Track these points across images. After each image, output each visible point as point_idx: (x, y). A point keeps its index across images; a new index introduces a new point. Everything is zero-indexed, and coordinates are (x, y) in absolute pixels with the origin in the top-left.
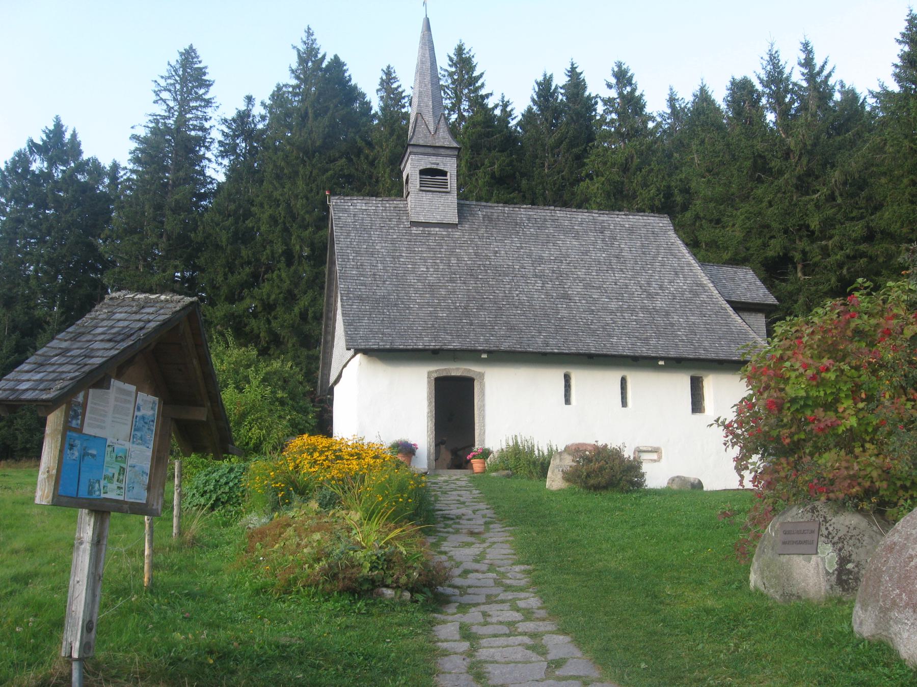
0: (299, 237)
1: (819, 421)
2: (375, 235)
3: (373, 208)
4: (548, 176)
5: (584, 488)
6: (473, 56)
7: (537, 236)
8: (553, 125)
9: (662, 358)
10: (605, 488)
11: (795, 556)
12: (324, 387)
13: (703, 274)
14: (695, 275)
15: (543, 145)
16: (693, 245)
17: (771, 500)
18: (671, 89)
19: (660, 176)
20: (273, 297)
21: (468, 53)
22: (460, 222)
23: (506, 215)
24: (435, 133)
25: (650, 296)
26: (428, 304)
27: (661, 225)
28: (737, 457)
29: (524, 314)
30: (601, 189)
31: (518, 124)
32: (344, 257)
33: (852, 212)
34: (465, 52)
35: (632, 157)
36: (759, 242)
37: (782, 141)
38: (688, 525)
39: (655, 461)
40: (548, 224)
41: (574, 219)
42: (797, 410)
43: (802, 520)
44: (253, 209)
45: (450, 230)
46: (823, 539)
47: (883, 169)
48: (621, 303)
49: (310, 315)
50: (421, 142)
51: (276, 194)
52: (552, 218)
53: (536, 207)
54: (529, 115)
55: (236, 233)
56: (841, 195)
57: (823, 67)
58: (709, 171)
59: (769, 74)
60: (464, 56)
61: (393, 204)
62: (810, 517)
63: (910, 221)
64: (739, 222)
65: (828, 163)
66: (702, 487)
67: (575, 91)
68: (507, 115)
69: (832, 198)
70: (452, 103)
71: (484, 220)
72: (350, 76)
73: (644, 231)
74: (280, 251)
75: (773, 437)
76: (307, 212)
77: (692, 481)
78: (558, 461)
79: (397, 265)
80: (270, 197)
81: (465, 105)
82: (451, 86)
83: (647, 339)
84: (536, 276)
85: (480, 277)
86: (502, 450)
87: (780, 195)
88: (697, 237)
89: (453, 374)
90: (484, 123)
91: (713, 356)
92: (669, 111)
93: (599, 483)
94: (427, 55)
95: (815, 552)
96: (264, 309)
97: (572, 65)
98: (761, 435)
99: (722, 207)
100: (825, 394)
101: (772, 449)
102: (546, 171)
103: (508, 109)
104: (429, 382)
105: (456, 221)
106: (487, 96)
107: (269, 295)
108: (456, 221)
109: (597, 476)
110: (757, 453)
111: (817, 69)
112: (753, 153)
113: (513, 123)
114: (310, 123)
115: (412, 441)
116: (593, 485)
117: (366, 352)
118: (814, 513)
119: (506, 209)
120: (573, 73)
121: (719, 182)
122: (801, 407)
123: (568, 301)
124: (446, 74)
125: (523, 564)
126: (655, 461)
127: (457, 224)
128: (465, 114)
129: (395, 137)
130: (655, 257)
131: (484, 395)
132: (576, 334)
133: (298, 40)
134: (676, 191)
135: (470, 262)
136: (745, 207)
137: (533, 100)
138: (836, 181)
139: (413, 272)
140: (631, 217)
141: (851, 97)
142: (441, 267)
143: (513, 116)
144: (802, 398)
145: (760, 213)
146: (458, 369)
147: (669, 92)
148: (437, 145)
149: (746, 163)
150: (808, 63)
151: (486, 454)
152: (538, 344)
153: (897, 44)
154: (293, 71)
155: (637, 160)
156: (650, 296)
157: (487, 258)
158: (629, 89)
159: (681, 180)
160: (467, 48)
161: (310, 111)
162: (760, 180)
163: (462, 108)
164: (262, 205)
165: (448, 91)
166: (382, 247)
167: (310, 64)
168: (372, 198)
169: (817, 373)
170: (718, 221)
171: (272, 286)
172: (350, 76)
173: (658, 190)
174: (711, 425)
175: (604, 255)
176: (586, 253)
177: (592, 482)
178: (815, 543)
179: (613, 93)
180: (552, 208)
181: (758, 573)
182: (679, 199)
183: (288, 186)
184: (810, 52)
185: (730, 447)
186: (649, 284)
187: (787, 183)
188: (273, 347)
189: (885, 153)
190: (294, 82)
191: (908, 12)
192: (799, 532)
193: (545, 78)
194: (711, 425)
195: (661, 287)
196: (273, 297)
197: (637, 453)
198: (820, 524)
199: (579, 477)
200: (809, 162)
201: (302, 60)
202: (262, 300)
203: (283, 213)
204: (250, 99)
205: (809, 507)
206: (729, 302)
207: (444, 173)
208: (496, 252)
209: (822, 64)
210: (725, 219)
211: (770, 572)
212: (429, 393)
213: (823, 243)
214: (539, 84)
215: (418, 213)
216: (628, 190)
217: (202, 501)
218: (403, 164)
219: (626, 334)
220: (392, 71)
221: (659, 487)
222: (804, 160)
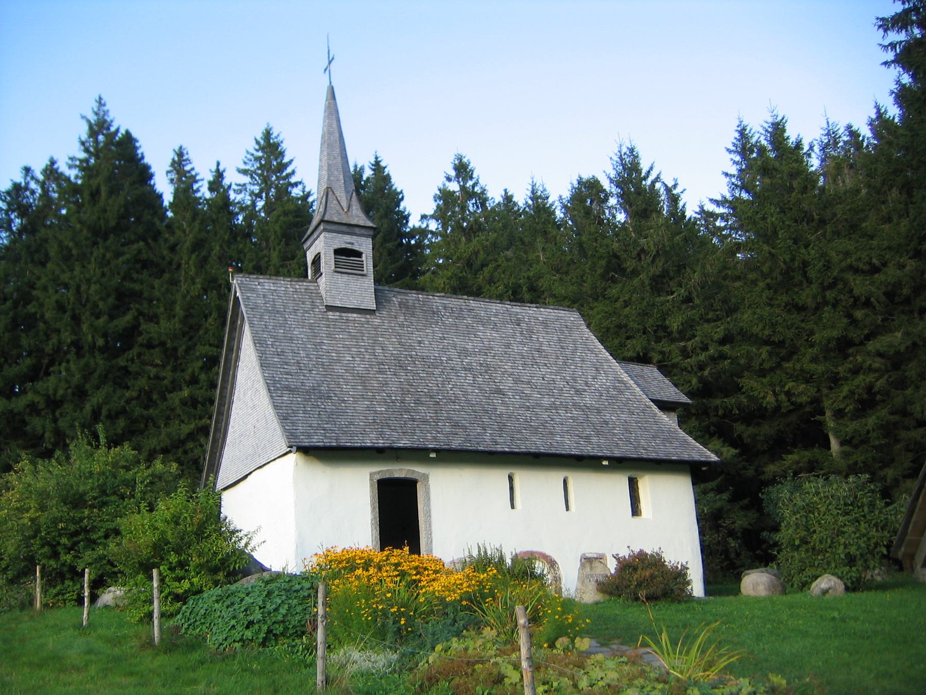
0: (91, 325)
3: (283, 289)
6: (282, 142)
9: (606, 458)
13: (622, 371)
20: (61, 392)
24: (348, 210)
25: (578, 392)
27: (572, 319)
32: (262, 342)
33: (708, 314)
40: (465, 313)
44: (34, 293)
48: (553, 400)
49: (104, 412)
50: (336, 219)
51: (65, 277)
55: (14, 319)
57: (649, 172)
61: (301, 286)
63: (772, 323)
69: (688, 300)
73: (557, 325)
76: (102, 299)
79: (320, 353)
89: (396, 476)
91: (653, 455)
96: (48, 406)
97: (377, 158)
104: (371, 485)
105: (374, 307)
108: (374, 307)
111: (643, 174)
117: (307, 451)
119: (420, 296)
123: (502, 396)
127: (374, 311)
129: (198, 222)
139: (339, 361)
140: (542, 309)
142: (367, 357)
146: (401, 470)
148: (352, 223)
149: (600, 262)
154: (83, 143)
155: (482, 255)
156: (578, 392)
162: (614, 281)
164: (45, 288)
166: (301, 333)
168: (279, 278)
171: (60, 380)
173: (506, 286)
176: (508, 346)
180: (465, 297)
183: (78, 269)
186: (575, 380)
191: (737, 123)
195: (586, 384)
196: (61, 392)
201: (93, 133)
202: (48, 396)
203: (72, 300)
204: (27, 170)
206: (652, 400)
207: (358, 254)
208: (420, 342)
209: (648, 169)
212: (372, 497)
213: (682, 344)
217: (248, 634)
219: (567, 432)
220: (185, 152)
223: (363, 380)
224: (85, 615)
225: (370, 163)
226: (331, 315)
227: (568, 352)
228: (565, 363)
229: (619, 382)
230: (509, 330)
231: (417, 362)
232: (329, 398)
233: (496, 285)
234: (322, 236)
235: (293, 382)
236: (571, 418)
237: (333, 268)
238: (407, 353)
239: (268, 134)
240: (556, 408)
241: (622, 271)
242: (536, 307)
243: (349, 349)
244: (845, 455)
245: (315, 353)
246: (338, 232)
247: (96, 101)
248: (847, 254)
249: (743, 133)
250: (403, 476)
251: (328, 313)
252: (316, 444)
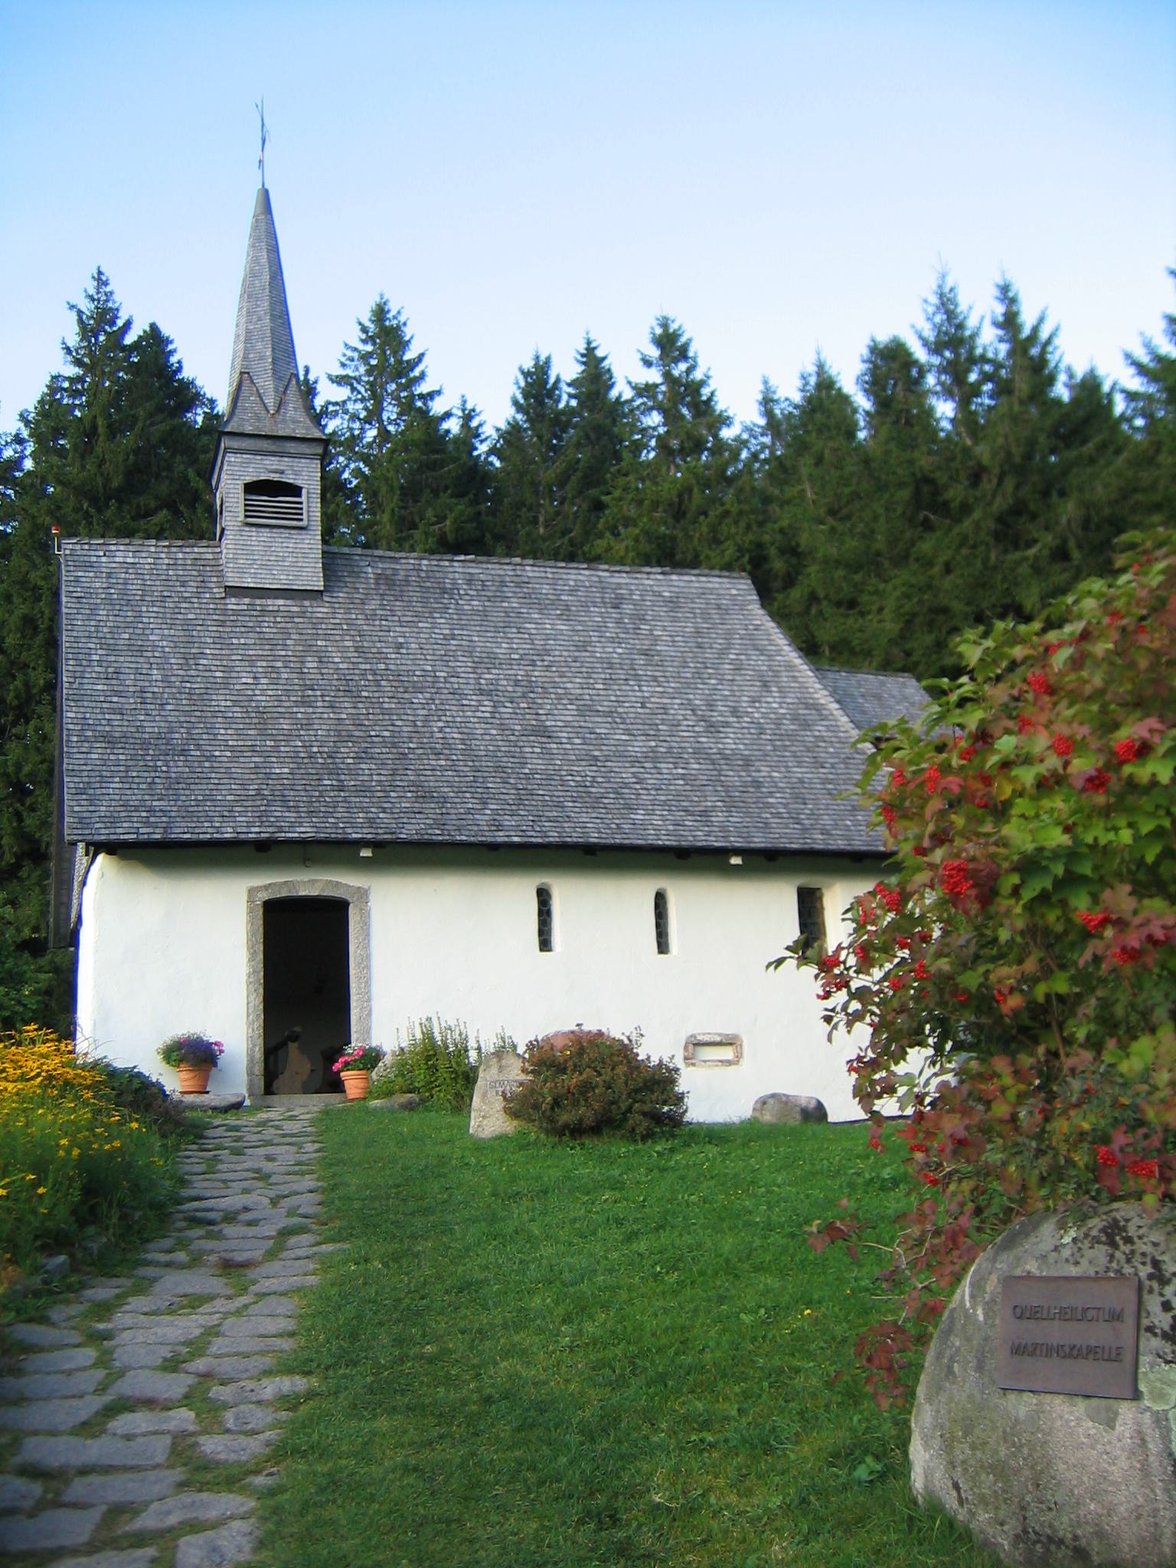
1: (1121, 924)
2: (150, 614)
3: (150, 560)
4: (544, 540)
5: (547, 1132)
6: (405, 324)
7: (485, 614)
8: (553, 448)
9: (737, 852)
10: (596, 1130)
11: (1058, 1400)
12: (62, 931)
13: (818, 686)
14: (803, 687)
15: (534, 484)
16: (810, 649)
17: (967, 1186)
18: (766, 382)
19: (742, 524)
21: (395, 317)
22: (328, 588)
23: (423, 574)
24: (278, 411)
26: (253, 749)
27: (734, 592)
28: (859, 1059)
29: (453, 767)
30: (634, 550)
31: (492, 451)
32: (81, 657)
34: (390, 316)
35: (690, 490)
36: (929, 639)
37: (966, 451)
38: (769, 1227)
39: (729, 1063)
41: (560, 582)
42: (1043, 898)
43: (1074, 1271)
45: (307, 603)
46: (1156, 1343)
47: (1156, 497)
48: (653, 744)
50: (249, 429)
52: (516, 579)
53: (484, 559)
54: (511, 435)
56: (1080, 547)
58: (832, 512)
59: (938, 328)
60: (387, 323)
62: (1103, 1260)
64: (890, 604)
65: (1052, 487)
66: (825, 1115)
67: (593, 388)
68: (471, 434)
70: (366, 409)
71: (377, 584)
72: (179, 362)
73: (699, 604)
74: (42, 682)
75: (966, 991)
77: (803, 1103)
78: (494, 1070)
79: (193, 673)
80: (24, 582)
81: (390, 412)
82: (365, 379)
83: (705, 813)
84: (482, 693)
85: (364, 694)
86: (402, 1049)
87: (964, 551)
88: (813, 636)
89: (302, 893)
90: (426, 444)
91: (841, 844)
92: (762, 422)
93: (581, 1121)
94: (264, 260)
95: (1129, 1394)
97: (589, 343)
98: (930, 988)
99: (857, 578)
100: (1137, 838)
101: (966, 1028)
102: (541, 530)
103: (474, 423)
104: (251, 911)
105: (320, 585)
106: (431, 395)
107: (19, 766)
108: (320, 585)
109: (576, 1104)
110: (922, 1044)
112: (913, 474)
113: (483, 448)
114: (101, 444)
115: (211, 1036)
116: (566, 1126)
118: (1113, 1245)
119: (425, 562)
120: (591, 359)
121: (851, 530)
122: (1059, 884)
123: (544, 740)
124: (356, 355)
125: (290, 1371)
126: (729, 1063)
127: (321, 592)
128: (391, 428)
130: (722, 653)
131: (368, 935)
132: (560, 806)
133: (79, 292)
134: (773, 551)
135: (345, 666)
136: (903, 576)
137: (516, 403)
138: (1069, 521)
139: (226, 685)
140: (674, 577)
141: (1089, 388)
143: (483, 437)
144: (1057, 854)
145: (929, 587)
146: (313, 882)
147: (762, 387)
148: (281, 433)
150: (1009, 322)
151: (371, 1058)
152: (480, 827)
156: (712, 728)
157: (382, 657)
158: (683, 366)
159: (782, 531)
160: (393, 308)
161: (100, 422)
162: (927, 526)
163: (385, 417)
165: (359, 387)
166: (163, 638)
167: (102, 338)
168: (147, 542)
169: (1108, 765)
170: (852, 604)
172: (179, 362)
173: (740, 549)
174: (779, 962)
175: (620, 651)
176: (584, 646)
177: (565, 1117)
178: (1128, 1357)
179: (654, 376)
180: (518, 560)
181: (937, 1443)
182: (778, 565)
184: (1013, 301)
185: (842, 1027)
186: (711, 706)
187: (977, 526)
188: (27, 863)
189: (1159, 467)
190: (73, 371)
192: (1067, 1315)
193: (536, 366)
194: (779, 962)
195: (734, 712)
197: (691, 1047)
198: (1140, 1288)
199: (536, 1107)
200: (1018, 487)
201: (87, 331)
205: (1096, 1224)
207: (295, 491)
208: (400, 646)
210: (864, 598)
211: (973, 1447)
212: (251, 934)
214: (526, 374)
215: (241, 571)
216: (683, 553)
218: (215, 476)
221: (736, 1120)
222: (1009, 484)
223: (263, 719)
225: (578, 352)
226: (232, 603)
227: (709, 654)
228: (698, 674)
229: (807, 706)
230: (596, 614)
231: (383, 683)
232: (184, 752)
233: (723, 547)
235: (118, 726)
236: (683, 777)
237: (241, 518)
238: (368, 666)
239: (380, 313)
240: (655, 760)
241: (942, 508)
242: (662, 573)
243: (252, 662)
245: (181, 672)
246: (256, 452)
247: (93, 277)
250: (316, 893)
251: (228, 601)
252: (122, 837)
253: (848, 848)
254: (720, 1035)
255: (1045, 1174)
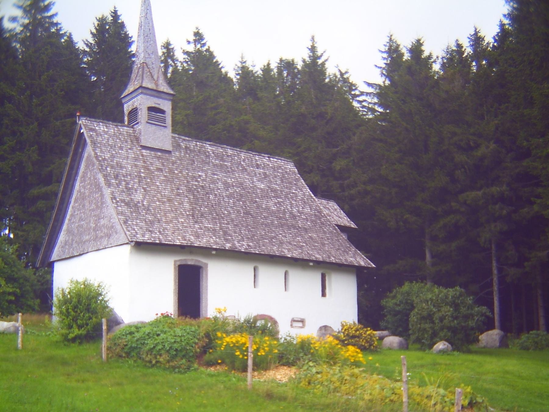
104: (175, 268)
108: (170, 148)
126: (302, 327)
146: (192, 260)
153: (90, 33)
207: (163, 112)
212: (175, 276)
224: (20, 340)
234: (139, 97)
244: (433, 265)
248: (454, 134)
249: (92, 33)
253: (341, 263)
254: (300, 318)
255: (442, 353)
